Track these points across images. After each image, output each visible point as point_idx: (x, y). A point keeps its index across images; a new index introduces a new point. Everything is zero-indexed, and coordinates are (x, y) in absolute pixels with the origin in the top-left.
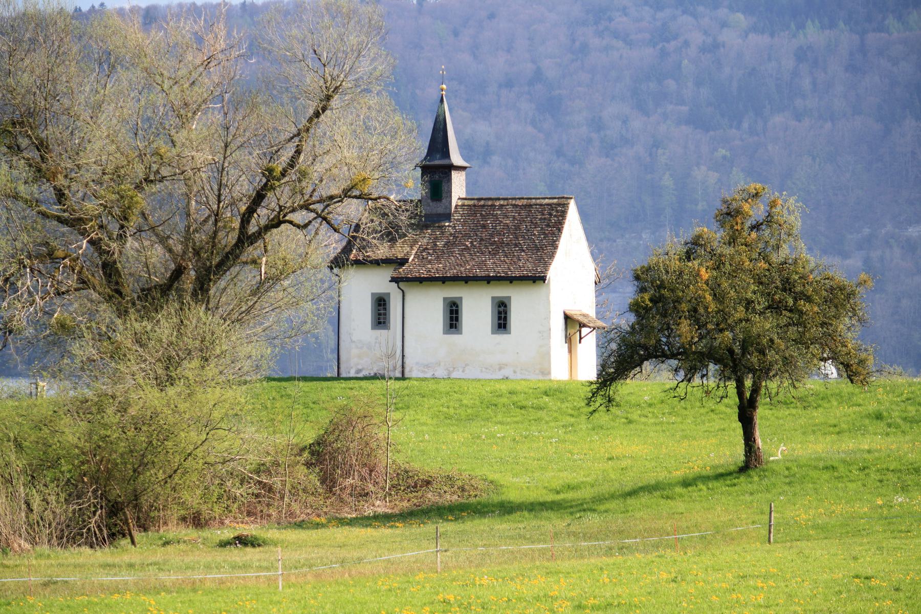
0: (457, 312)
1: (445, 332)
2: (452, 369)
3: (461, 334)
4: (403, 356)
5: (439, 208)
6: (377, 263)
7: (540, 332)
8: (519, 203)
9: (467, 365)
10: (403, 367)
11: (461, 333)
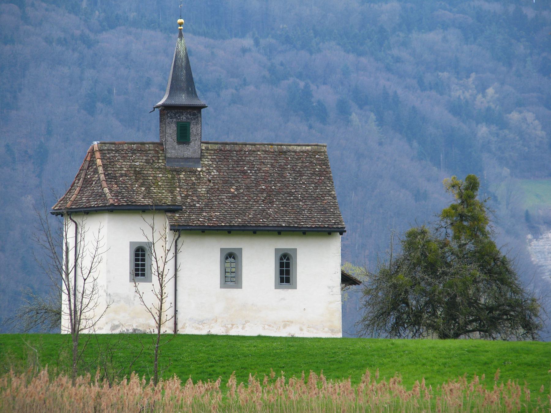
2: (230, 326)
3: (241, 288)
7: (329, 287)
8: (268, 148)
11: (295, 288)
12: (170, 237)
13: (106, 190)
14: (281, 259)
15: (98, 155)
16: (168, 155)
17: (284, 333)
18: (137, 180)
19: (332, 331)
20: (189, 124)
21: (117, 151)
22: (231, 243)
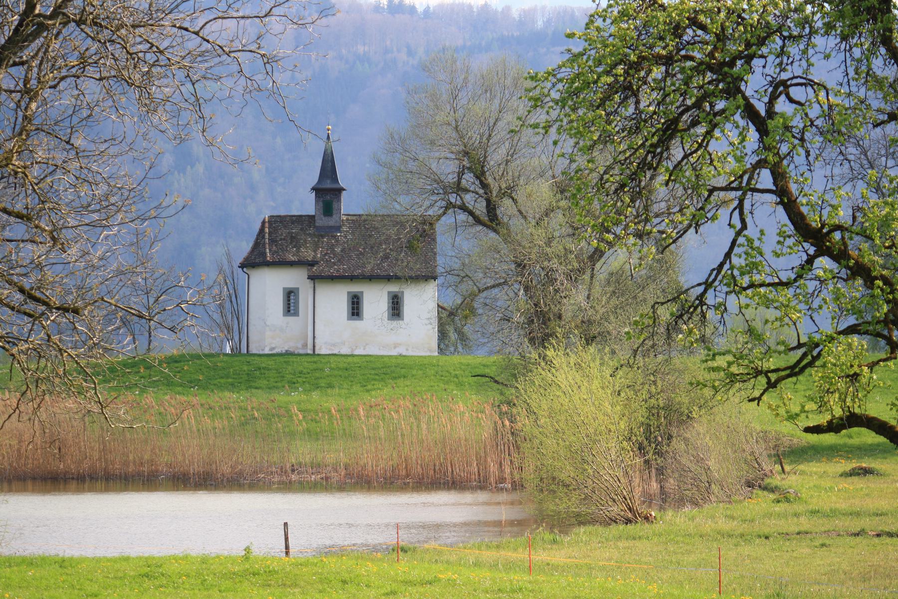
0: (358, 303)
1: (349, 319)
4: (314, 337)
5: (331, 222)
6: (291, 264)
9: (367, 344)
10: (314, 346)
12: (309, 284)
13: (268, 250)
14: (393, 299)
15: (267, 225)
16: (317, 224)
17: (394, 353)
18: (291, 243)
19: (430, 351)
20: (332, 202)
21: (281, 222)
22: (355, 288)
